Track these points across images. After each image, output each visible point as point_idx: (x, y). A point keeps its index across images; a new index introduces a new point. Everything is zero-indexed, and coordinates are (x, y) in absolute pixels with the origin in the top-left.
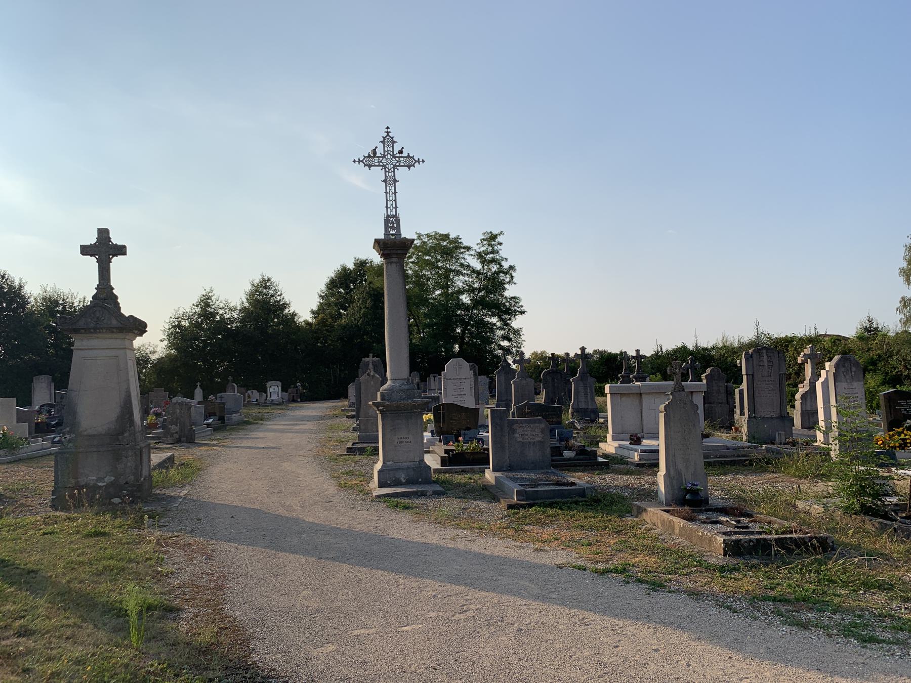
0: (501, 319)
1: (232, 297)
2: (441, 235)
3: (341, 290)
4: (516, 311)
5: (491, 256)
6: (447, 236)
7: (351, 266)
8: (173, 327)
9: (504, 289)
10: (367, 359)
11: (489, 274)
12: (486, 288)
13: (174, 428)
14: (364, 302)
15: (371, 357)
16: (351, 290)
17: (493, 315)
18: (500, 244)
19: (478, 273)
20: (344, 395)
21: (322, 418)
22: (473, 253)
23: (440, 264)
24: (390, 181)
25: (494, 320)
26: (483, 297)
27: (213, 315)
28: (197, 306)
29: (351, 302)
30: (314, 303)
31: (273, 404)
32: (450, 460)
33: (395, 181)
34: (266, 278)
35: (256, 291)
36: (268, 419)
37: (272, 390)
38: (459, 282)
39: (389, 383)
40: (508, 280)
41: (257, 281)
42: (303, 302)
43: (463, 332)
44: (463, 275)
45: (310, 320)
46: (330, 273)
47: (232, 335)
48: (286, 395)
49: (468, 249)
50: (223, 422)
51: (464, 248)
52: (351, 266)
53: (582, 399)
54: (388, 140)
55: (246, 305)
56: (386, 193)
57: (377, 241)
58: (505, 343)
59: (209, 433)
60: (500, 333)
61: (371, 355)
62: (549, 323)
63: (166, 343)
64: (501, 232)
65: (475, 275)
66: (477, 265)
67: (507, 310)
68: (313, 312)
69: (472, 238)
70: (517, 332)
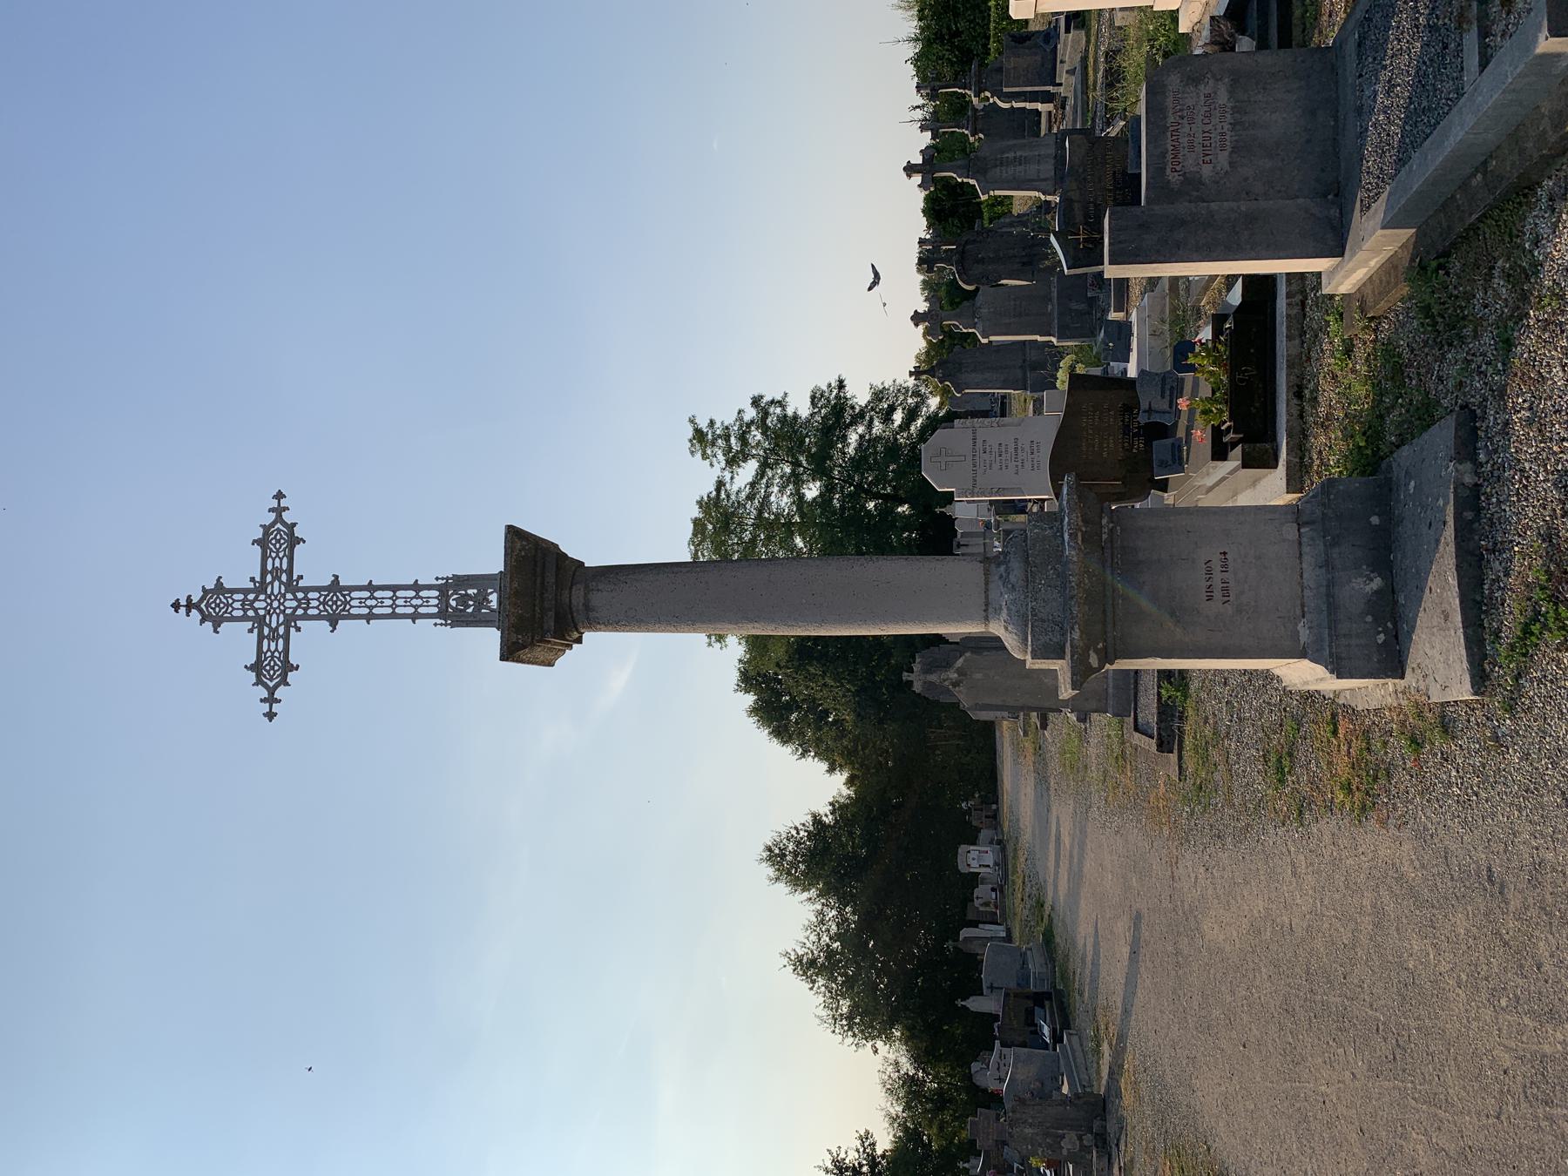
0: (854, 422)
1: (797, 917)
2: (695, 535)
3: (793, 717)
4: (838, 397)
5: (733, 440)
6: (696, 522)
7: (750, 699)
8: (850, 1028)
9: (796, 417)
10: (917, 688)
11: (766, 445)
12: (790, 451)
13: (1069, 1142)
14: (812, 678)
15: (912, 677)
16: (793, 698)
17: (845, 438)
18: (712, 423)
19: (764, 465)
20: (989, 729)
21: (1042, 779)
22: (727, 475)
23: (747, 536)
24: (336, 604)
25: (853, 438)
26: (810, 458)
27: (830, 953)
28: (813, 982)
29: (812, 701)
30: (815, 767)
31: (1003, 863)
32: (1250, 433)
33: (335, 586)
34: (766, 854)
35: (789, 873)
36: (1041, 888)
37: (974, 864)
38: (782, 501)
39: (997, 629)
40: (778, 410)
41: (771, 871)
42: (811, 788)
43: (875, 496)
44: (767, 495)
45: (846, 775)
46: (760, 737)
47: (869, 923)
48: (985, 834)
49: (720, 484)
50: (1048, 995)
51: (718, 490)
52: (750, 699)
53: (1032, 170)
54: (211, 606)
55: (813, 893)
56: (369, 617)
57: (510, 652)
58: (898, 417)
59: (1075, 1039)
60: (878, 428)
61: (906, 676)
62: (857, 328)
63: (879, 1044)
64: (692, 421)
65: (770, 473)
66: (749, 469)
67: (835, 411)
68: (831, 770)
69: (702, 476)
70: (878, 395)
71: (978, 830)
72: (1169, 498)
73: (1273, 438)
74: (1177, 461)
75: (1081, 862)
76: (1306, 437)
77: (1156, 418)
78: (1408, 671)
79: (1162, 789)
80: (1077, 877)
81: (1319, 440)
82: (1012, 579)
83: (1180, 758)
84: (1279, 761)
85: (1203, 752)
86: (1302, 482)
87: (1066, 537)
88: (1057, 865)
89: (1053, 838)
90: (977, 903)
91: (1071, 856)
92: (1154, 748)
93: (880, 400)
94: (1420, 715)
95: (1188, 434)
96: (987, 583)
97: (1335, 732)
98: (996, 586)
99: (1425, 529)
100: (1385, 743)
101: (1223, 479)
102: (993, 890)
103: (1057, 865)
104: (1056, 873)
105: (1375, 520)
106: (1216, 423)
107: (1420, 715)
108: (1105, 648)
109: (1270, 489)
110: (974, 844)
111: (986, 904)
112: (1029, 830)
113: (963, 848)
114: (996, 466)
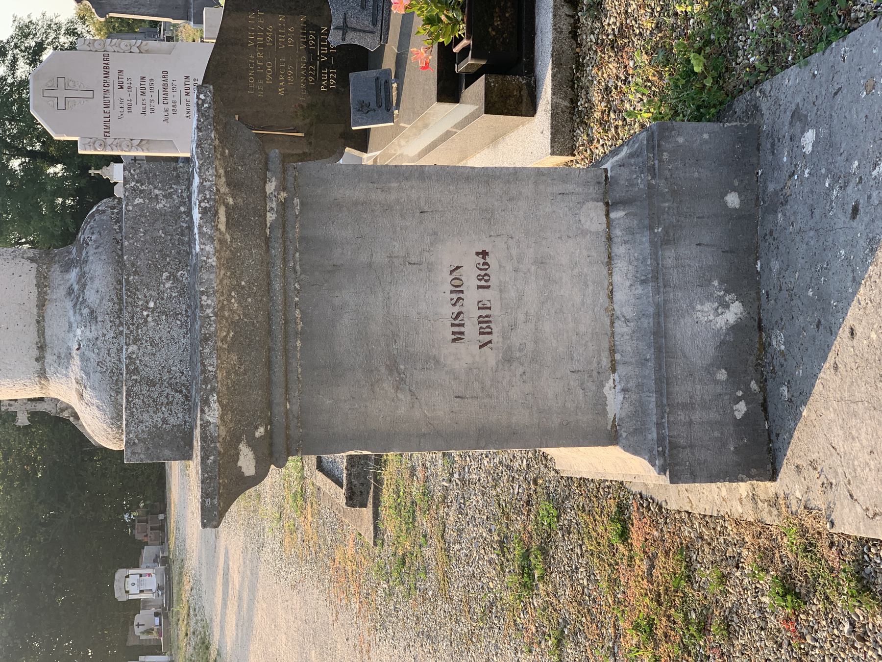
31: (167, 587)
37: (134, 590)
48: (148, 552)
71: (142, 544)
72: (367, 158)
73: (530, 69)
74: (383, 105)
75: (251, 609)
76: (580, 67)
77: (353, 39)
78: (786, 472)
79: (350, 549)
80: (246, 625)
81: (605, 71)
82: (91, 296)
83: (376, 515)
84: (526, 556)
85: (409, 513)
86: (574, 139)
87: (196, 215)
88: (225, 605)
89: (221, 572)
90: (137, 631)
91: (240, 599)
92: (342, 500)
93: (26, 36)
94: (809, 548)
95: (401, 61)
96: (42, 304)
97: (624, 535)
98: (61, 310)
99: (841, 219)
100: (724, 578)
101: (448, 135)
102: (157, 614)
103: (225, 605)
104: (224, 615)
105: (733, 200)
106: (446, 40)
107: (809, 548)
108: (269, 434)
109: (526, 143)
110: (137, 566)
111: (149, 631)
112: (195, 555)
113: (120, 573)
114: (137, 109)
